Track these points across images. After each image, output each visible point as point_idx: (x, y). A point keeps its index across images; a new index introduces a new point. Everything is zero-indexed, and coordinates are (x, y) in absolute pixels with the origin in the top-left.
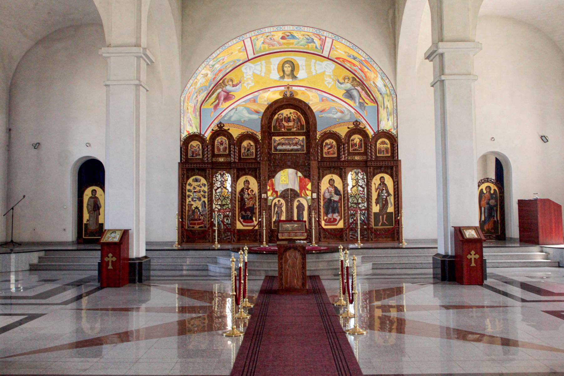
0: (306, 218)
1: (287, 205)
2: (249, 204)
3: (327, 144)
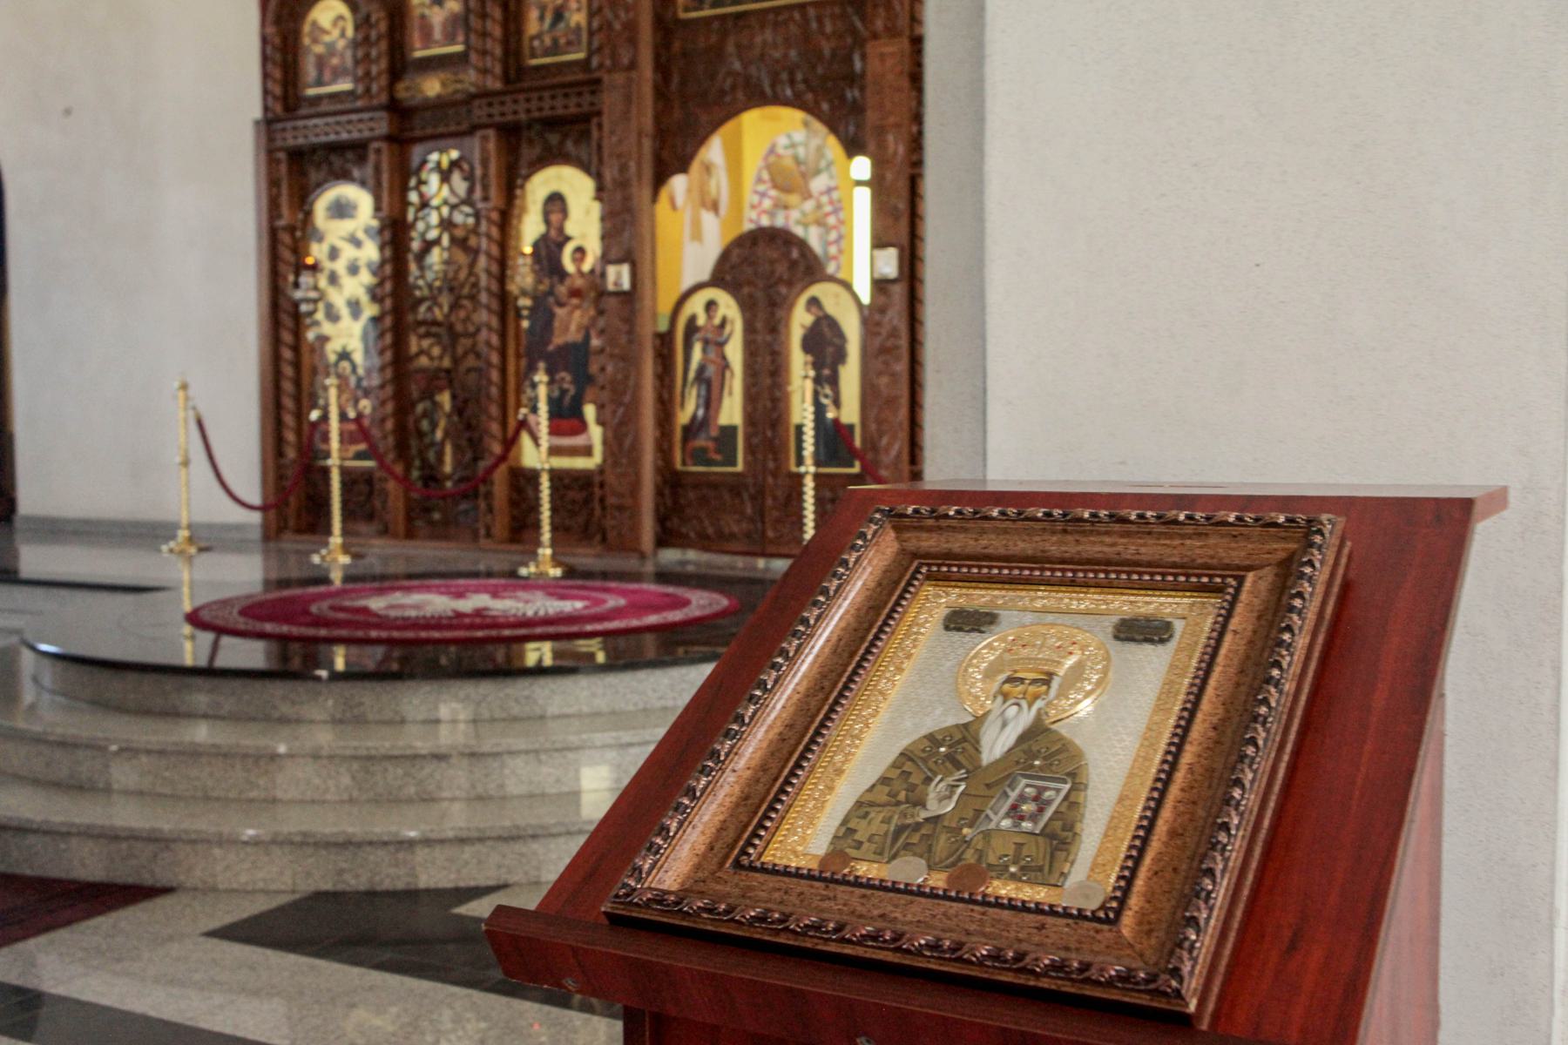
1: (749, 329)
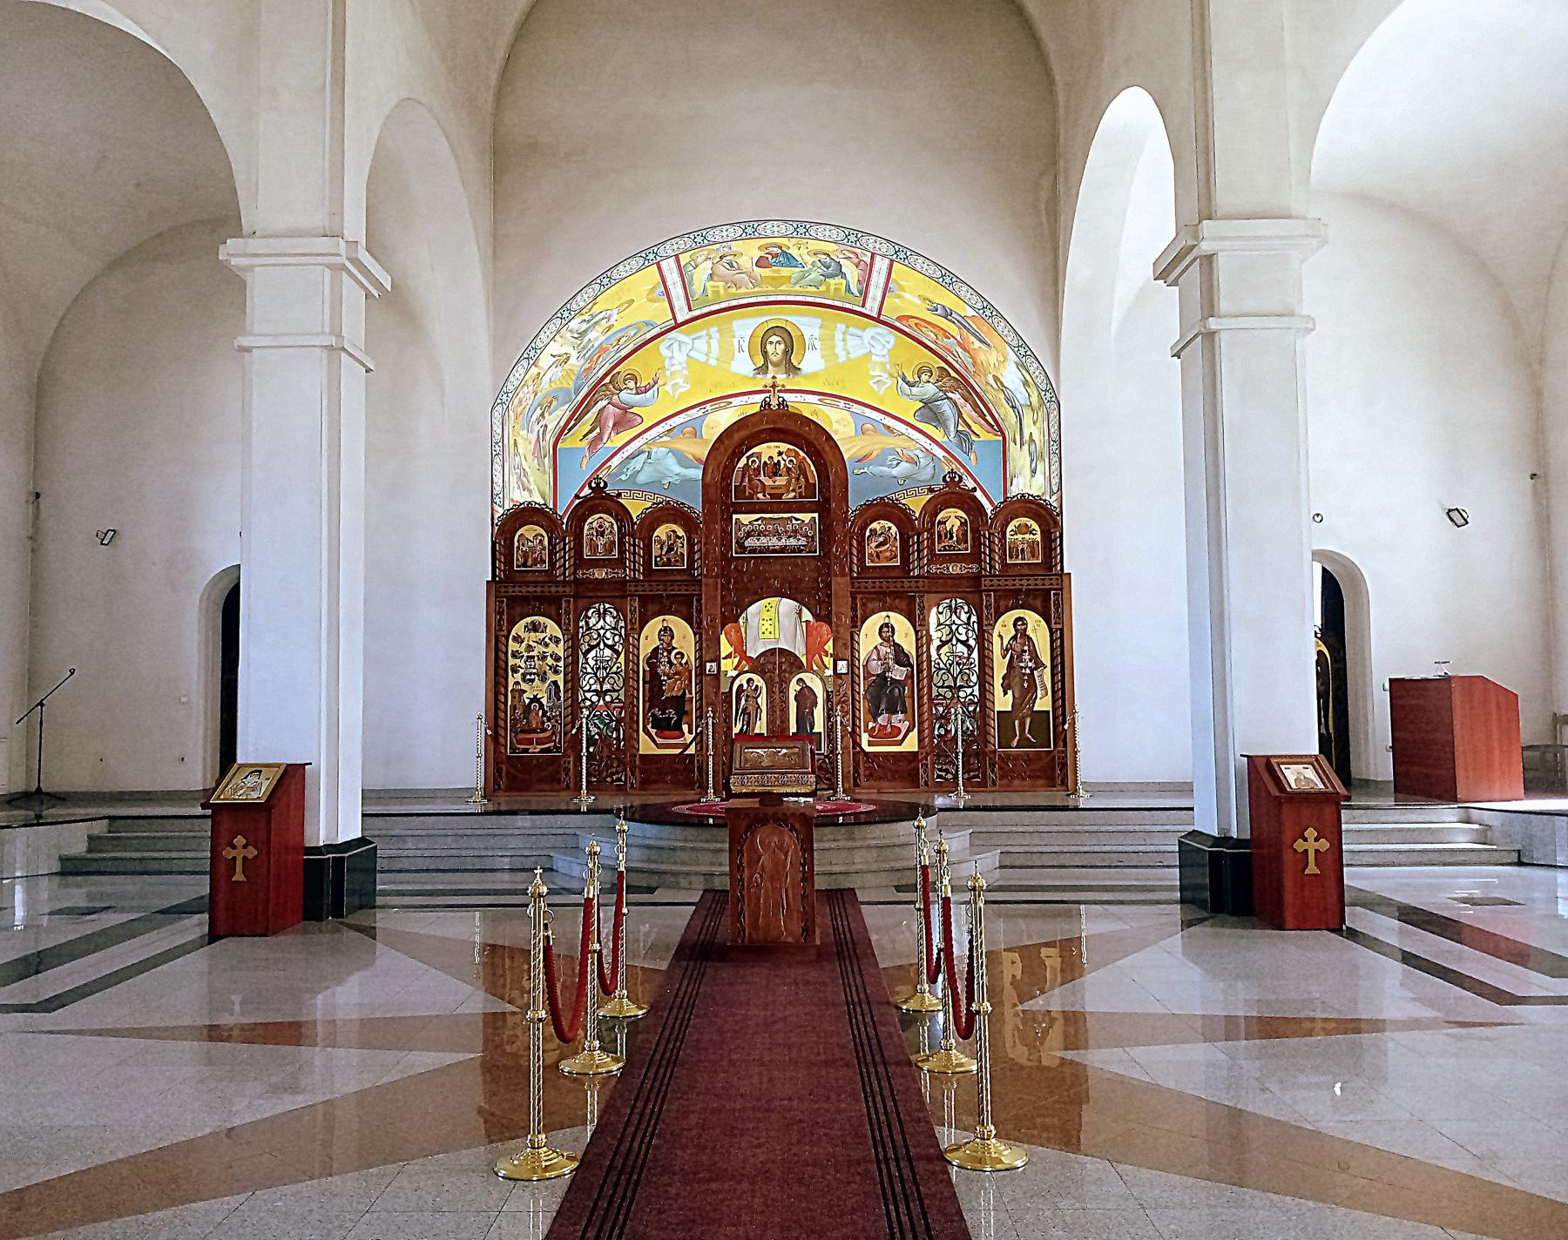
0: (819, 727)
2: (671, 689)
3: (873, 532)
